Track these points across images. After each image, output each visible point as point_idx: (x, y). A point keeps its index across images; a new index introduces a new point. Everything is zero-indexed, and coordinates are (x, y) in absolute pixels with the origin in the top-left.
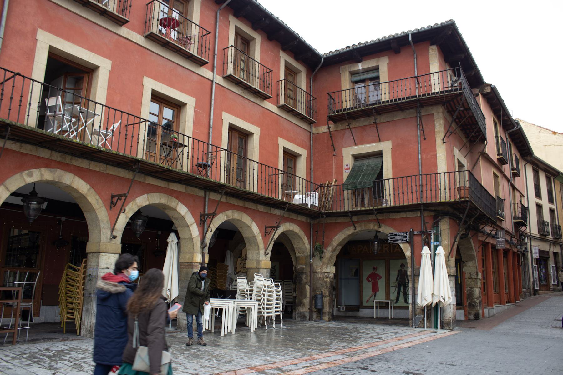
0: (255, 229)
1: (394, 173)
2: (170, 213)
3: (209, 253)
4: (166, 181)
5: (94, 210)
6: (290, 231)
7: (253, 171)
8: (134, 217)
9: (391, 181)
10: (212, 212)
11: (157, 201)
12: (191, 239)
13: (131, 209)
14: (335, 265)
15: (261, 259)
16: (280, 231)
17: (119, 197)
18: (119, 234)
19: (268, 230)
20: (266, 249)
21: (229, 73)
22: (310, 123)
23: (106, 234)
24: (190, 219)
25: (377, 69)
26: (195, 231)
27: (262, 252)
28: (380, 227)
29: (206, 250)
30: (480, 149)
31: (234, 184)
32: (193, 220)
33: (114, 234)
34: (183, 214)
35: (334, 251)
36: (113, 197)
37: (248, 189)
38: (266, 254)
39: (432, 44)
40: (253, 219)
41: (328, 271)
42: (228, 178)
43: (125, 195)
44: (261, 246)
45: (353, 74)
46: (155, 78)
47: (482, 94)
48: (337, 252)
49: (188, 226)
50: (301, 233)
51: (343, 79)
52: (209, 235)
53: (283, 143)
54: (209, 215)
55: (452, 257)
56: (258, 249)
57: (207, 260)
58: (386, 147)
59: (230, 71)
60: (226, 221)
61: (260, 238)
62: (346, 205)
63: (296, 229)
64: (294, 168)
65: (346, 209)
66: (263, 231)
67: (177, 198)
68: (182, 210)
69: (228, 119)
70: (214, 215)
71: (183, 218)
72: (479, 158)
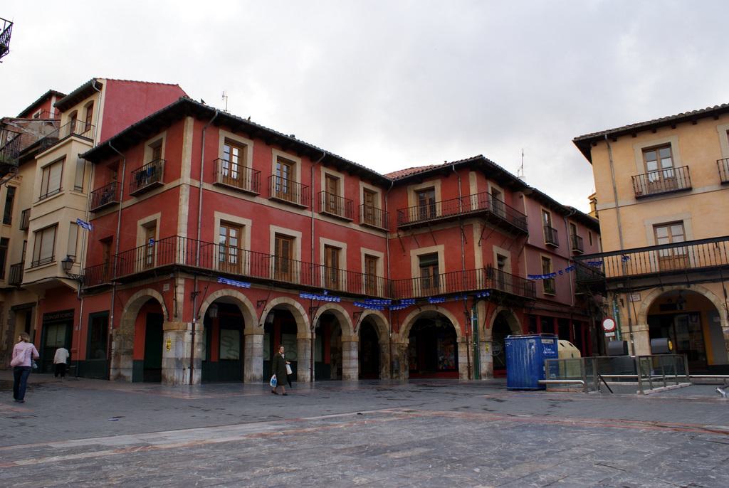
0: (346, 314)
1: (446, 270)
2: (290, 309)
3: (316, 332)
4: (284, 296)
5: (248, 310)
6: (372, 314)
7: (343, 276)
8: (210, 307)
9: (419, 279)
10: (316, 306)
11: (283, 302)
12: (304, 324)
13: (269, 307)
14: (409, 337)
15: (351, 335)
16: (365, 314)
17: (262, 301)
18: (263, 322)
19: (356, 314)
20: (355, 328)
21: (322, 211)
22: (385, 232)
23: (256, 323)
24: (302, 311)
25: (432, 189)
26: (306, 318)
27: (352, 330)
28: (437, 309)
29: (314, 331)
30: (524, 241)
31: (332, 287)
32: (305, 312)
33: (261, 323)
34: (298, 308)
35: (407, 327)
36: (258, 302)
37: (341, 290)
38: (355, 332)
39: (471, 171)
40: (345, 308)
41: (403, 342)
42: (326, 283)
43: (266, 301)
44: (351, 326)
45: (418, 192)
46: (277, 224)
47: (526, 196)
48: (410, 328)
49: (301, 316)
50: (382, 316)
51: (409, 196)
52: (315, 321)
53: (364, 251)
54: (314, 308)
55: (488, 328)
56: (349, 328)
57: (315, 337)
58: (440, 249)
59: (323, 209)
60: (326, 311)
61: (350, 321)
62: (478, 285)
63: (377, 312)
64: (375, 268)
65: (478, 288)
66: (308, 311)
67: (294, 298)
68: (298, 305)
69: (324, 241)
70: (318, 308)
71: (298, 311)
72: (523, 249)
